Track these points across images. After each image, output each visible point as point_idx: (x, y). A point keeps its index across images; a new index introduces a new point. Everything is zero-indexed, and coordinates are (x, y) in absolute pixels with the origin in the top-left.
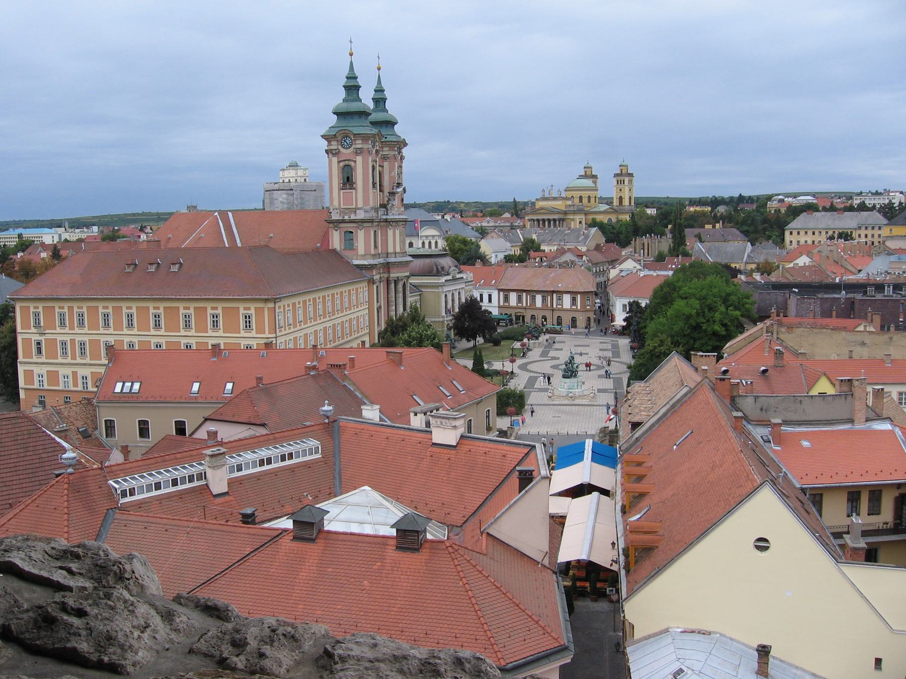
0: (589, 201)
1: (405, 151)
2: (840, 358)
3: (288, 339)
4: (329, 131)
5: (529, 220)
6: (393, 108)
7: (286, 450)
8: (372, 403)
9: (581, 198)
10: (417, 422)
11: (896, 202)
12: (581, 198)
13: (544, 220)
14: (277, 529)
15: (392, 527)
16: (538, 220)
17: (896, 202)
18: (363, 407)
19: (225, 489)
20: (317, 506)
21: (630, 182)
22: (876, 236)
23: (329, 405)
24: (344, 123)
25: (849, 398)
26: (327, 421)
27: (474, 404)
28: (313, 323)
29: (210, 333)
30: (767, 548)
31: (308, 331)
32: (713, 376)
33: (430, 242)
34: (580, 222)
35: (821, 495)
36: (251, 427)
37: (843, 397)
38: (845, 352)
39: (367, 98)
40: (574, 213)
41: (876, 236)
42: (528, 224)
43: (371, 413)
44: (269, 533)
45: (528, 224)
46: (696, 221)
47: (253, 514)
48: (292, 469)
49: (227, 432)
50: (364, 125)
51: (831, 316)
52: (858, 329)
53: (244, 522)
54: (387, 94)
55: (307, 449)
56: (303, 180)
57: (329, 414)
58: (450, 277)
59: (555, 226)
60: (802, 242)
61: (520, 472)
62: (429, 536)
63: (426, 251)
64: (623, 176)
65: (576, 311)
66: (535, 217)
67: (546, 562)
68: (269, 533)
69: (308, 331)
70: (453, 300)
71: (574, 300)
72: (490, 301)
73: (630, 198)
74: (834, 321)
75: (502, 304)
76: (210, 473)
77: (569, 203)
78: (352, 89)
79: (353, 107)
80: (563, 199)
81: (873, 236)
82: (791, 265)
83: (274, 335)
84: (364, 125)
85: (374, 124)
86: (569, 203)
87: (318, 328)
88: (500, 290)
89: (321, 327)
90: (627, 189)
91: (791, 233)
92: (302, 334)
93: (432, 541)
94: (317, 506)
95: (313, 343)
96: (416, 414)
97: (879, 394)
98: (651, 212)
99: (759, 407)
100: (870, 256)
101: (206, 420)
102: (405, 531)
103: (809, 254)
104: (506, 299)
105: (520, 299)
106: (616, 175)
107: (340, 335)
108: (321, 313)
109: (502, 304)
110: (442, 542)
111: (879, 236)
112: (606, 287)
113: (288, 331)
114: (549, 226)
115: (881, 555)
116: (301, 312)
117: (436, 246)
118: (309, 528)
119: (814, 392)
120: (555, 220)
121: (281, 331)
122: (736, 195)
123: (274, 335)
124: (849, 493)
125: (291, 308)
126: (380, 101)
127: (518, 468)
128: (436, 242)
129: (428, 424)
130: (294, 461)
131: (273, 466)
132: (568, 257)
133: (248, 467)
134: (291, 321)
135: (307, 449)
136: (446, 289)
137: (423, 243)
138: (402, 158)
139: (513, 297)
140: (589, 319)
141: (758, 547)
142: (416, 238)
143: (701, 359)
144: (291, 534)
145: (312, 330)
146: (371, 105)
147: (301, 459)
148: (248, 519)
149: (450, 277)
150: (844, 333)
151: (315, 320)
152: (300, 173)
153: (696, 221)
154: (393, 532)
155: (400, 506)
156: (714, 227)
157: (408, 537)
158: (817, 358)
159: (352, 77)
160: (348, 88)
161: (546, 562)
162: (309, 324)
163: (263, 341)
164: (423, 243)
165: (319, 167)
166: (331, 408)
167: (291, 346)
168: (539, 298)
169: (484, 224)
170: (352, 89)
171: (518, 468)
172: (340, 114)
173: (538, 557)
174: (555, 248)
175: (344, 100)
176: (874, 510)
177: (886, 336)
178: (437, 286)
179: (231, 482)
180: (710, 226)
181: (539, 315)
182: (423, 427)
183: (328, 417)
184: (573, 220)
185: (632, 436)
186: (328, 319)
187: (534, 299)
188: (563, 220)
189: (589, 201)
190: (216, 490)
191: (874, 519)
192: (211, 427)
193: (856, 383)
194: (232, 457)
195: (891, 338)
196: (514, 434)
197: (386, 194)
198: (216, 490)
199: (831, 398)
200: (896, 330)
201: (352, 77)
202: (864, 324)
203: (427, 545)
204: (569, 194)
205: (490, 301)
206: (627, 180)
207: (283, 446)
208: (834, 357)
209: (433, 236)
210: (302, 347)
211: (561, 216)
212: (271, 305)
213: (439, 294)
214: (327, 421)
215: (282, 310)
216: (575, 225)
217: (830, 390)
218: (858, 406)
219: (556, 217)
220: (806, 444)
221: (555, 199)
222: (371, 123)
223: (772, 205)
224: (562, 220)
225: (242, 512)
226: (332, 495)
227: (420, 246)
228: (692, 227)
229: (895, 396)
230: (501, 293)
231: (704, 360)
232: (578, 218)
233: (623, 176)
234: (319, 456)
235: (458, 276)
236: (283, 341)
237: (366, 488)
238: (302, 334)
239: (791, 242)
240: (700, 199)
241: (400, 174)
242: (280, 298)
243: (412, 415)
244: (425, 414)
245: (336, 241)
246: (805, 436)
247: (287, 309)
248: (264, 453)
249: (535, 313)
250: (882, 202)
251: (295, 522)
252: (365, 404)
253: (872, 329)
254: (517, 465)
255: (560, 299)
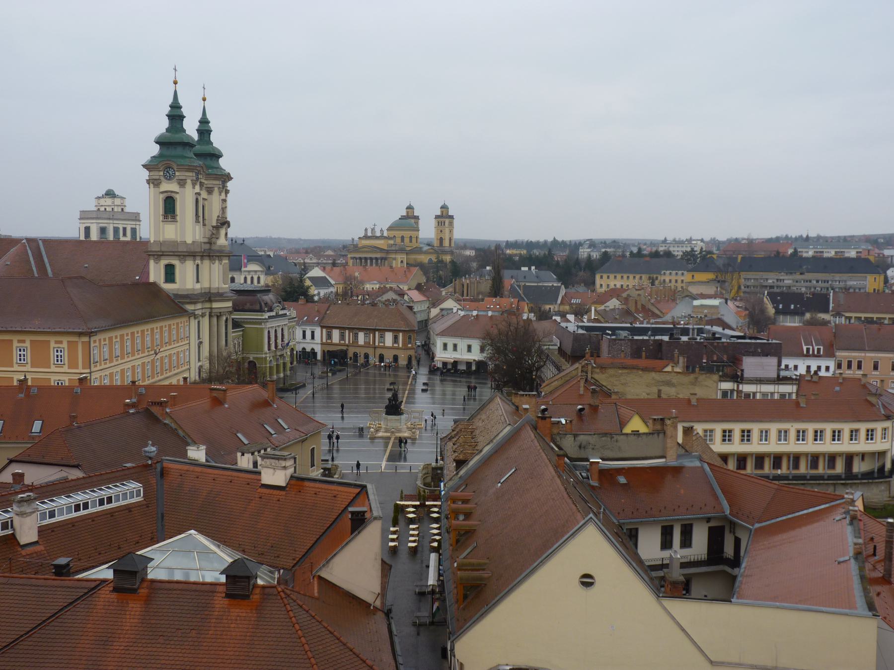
0: (411, 241)
1: (230, 185)
2: (649, 397)
3: (103, 374)
4: (151, 161)
5: (352, 258)
6: (217, 140)
7: (105, 493)
8: (195, 443)
9: (403, 238)
10: (245, 462)
11: (697, 249)
12: (403, 238)
13: (366, 259)
14: (95, 580)
15: (221, 573)
16: (360, 259)
17: (697, 249)
18: (188, 448)
19: (35, 538)
20: (139, 553)
21: (451, 224)
22: (679, 281)
23: (153, 445)
24: (168, 152)
25: (661, 435)
26: (150, 462)
27: (299, 442)
28: (130, 359)
29: (53, 369)
30: (591, 584)
31: (125, 366)
32: (531, 416)
33: (252, 278)
34: (402, 262)
35: (637, 530)
36: (62, 468)
37: (656, 435)
38: (655, 390)
39: (191, 128)
40: (396, 252)
41: (679, 281)
42: (351, 262)
43: (198, 453)
44: (84, 584)
45: (351, 262)
46: (513, 264)
47: (68, 565)
48: (111, 513)
49: (35, 475)
50: (187, 154)
51: (640, 357)
52: (666, 369)
53: (56, 574)
54: (212, 125)
55: (128, 493)
56: (120, 210)
57: (152, 455)
58: (273, 314)
59: (377, 264)
60: (618, 286)
61: (353, 513)
62: (260, 582)
63: (248, 286)
64: (444, 217)
65: (398, 348)
66: (358, 255)
67: (378, 604)
68: (84, 584)
69: (125, 366)
70: (283, 335)
71: (396, 339)
72: (313, 337)
73: (450, 239)
74: (643, 362)
75: (324, 341)
76: (17, 521)
77: (391, 242)
78: (176, 116)
79: (177, 137)
80: (385, 238)
81: (676, 281)
82: (603, 307)
83: (88, 371)
84: (187, 154)
85: (198, 155)
86: (391, 242)
87: (137, 363)
88: (322, 327)
89: (139, 362)
90: (447, 231)
91: (601, 277)
92: (118, 369)
93: (263, 587)
94: (139, 553)
95: (130, 379)
96: (243, 455)
97: (688, 431)
98: (468, 253)
99: (578, 443)
100: (674, 300)
101: (11, 461)
102: (235, 577)
103: (618, 297)
104: (329, 336)
105: (342, 337)
106: (437, 217)
107: (159, 370)
108: (129, 351)
109: (324, 341)
110: (274, 587)
111: (682, 281)
112: (426, 326)
113: (103, 366)
114: (371, 264)
115: (695, 588)
116: (118, 346)
117: (259, 282)
118: (130, 578)
119: (627, 430)
120: (377, 259)
121: (96, 366)
122: (550, 239)
123: (88, 371)
124: (663, 527)
125: (107, 342)
126: (204, 130)
127: (350, 509)
128: (259, 278)
129: (255, 464)
130: (114, 505)
131: (91, 510)
132: (390, 295)
133: (61, 514)
134: (107, 356)
135: (128, 493)
136: (269, 325)
137: (245, 278)
138: (227, 192)
139: (336, 334)
140: (410, 359)
141: (583, 583)
142: (238, 273)
143: (522, 398)
144: (112, 585)
145: (129, 365)
146: (195, 136)
147: (122, 503)
148: (61, 571)
149: (273, 314)
150: (653, 374)
151: (133, 355)
152: (117, 201)
153: (513, 264)
154: (223, 579)
155: (229, 550)
156: (530, 269)
157: (238, 582)
158: (629, 397)
159: (175, 106)
160: (171, 117)
161: (378, 604)
162: (115, 363)
163: (77, 377)
164: (245, 278)
165: (140, 198)
166: (154, 449)
167: (107, 382)
168: (361, 335)
169: (307, 261)
170: (176, 116)
171: (350, 509)
172: (160, 142)
173: (368, 598)
174: (377, 286)
175: (167, 130)
176: (686, 542)
177: (692, 376)
178: (260, 322)
179: (42, 530)
180: (526, 269)
181: (361, 352)
182: (250, 467)
183: (150, 458)
184: (395, 259)
185: (457, 474)
186: (147, 354)
187: (356, 337)
188: (385, 259)
189: (411, 241)
190: (23, 541)
191: (686, 552)
192: (18, 469)
193: (668, 422)
194: (43, 503)
195: (696, 378)
196: (338, 473)
197: (209, 227)
198: (23, 541)
199: (644, 437)
200: (700, 370)
201: (175, 106)
202: (672, 364)
203: (257, 591)
204: (392, 234)
205: (313, 337)
206: (447, 221)
207: (101, 489)
208: (644, 396)
209: (256, 272)
210: (119, 383)
211: (383, 255)
212: (86, 339)
213: (262, 329)
214: (150, 462)
215: (97, 344)
216: (397, 264)
217: (643, 429)
218: (670, 443)
219: (378, 255)
220: (622, 480)
221: (377, 238)
222: (196, 155)
223: (584, 253)
224: (384, 259)
225: (54, 563)
226: (154, 541)
227: (242, 281)
228: (507, 268)
229: (701, 433)
230: (324, 330)
231: (525, 399)
232: (400, 257)
233: (444, 217)
234: (140, 499)
235: (281, 312)
236: (98, 376)
237: (192, 532)
238: (130, 366)
239: (601, 285)
240: (787, 236)
241: (224, 209)
242: (96, 332)
243: (239, 454)
244: (253, 454)
245: (156, 273)
246: (620, 471)
247: (103, 343)
248: (79, 497)
249: (358, 350)
250: (684, 249)
251: (116, 572)
252: (189, 445)
253: (678, 370)
254: (348, 505)
255: (382, 337)
